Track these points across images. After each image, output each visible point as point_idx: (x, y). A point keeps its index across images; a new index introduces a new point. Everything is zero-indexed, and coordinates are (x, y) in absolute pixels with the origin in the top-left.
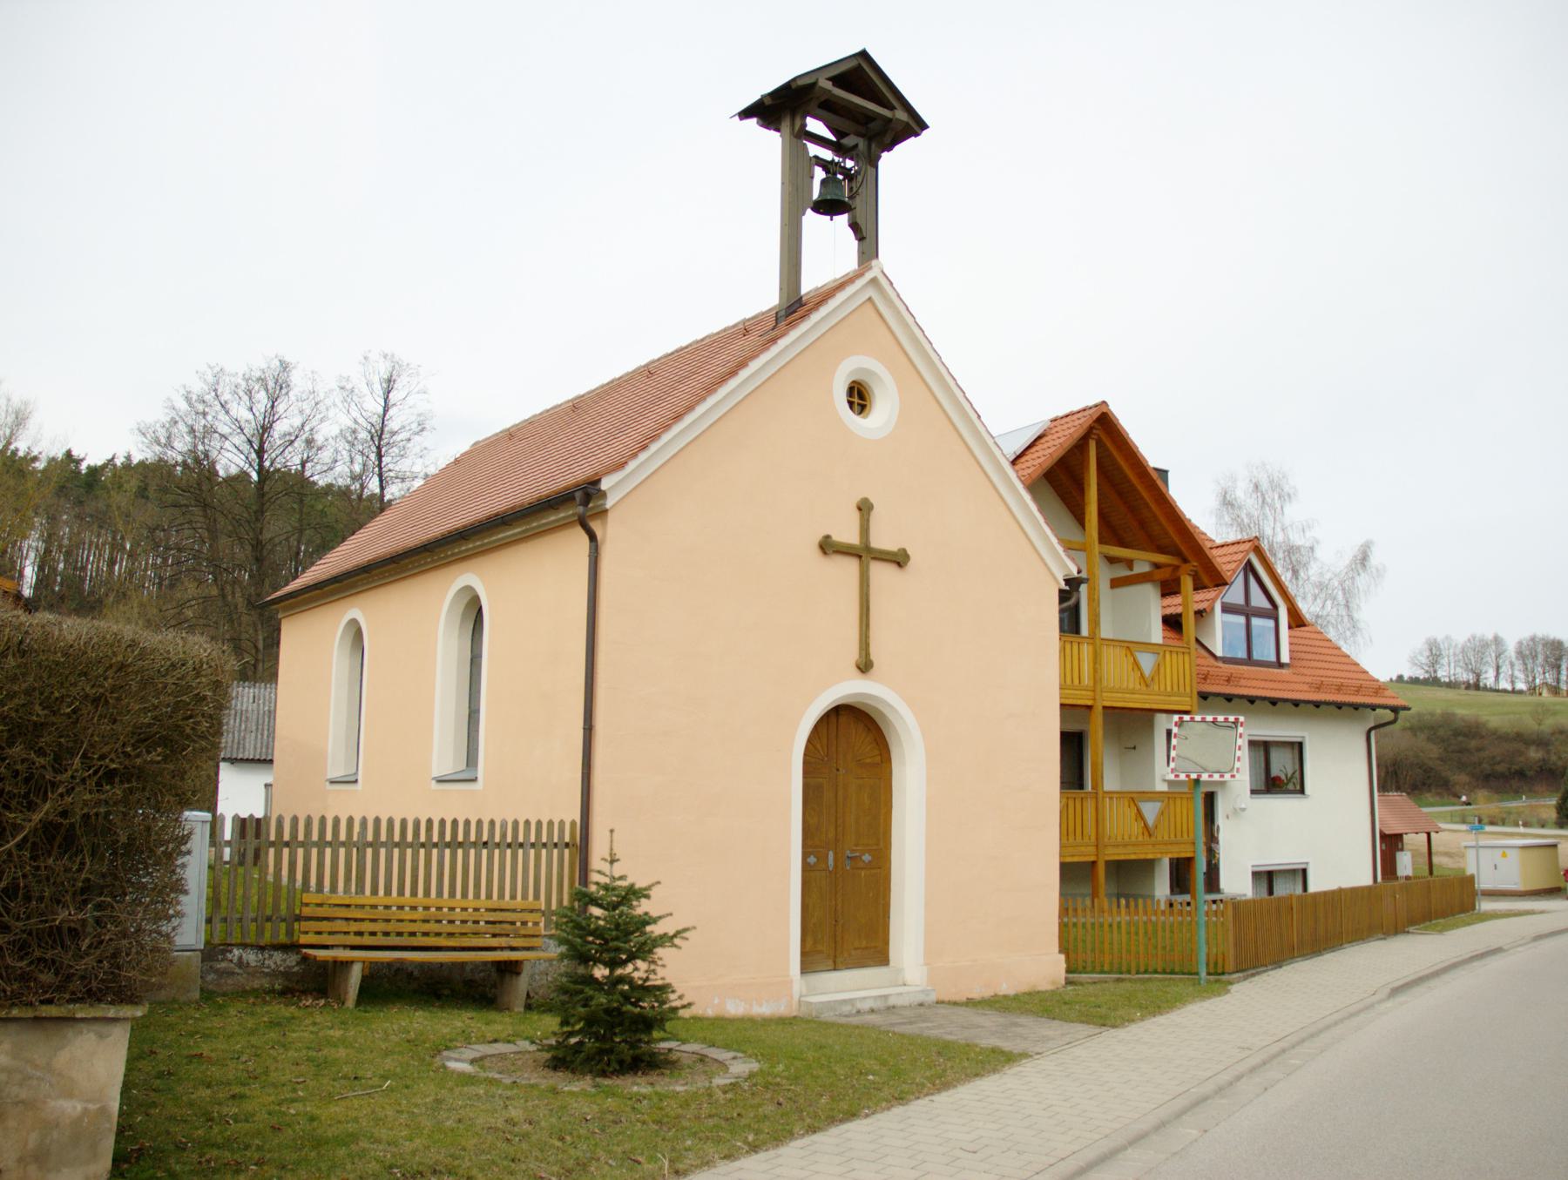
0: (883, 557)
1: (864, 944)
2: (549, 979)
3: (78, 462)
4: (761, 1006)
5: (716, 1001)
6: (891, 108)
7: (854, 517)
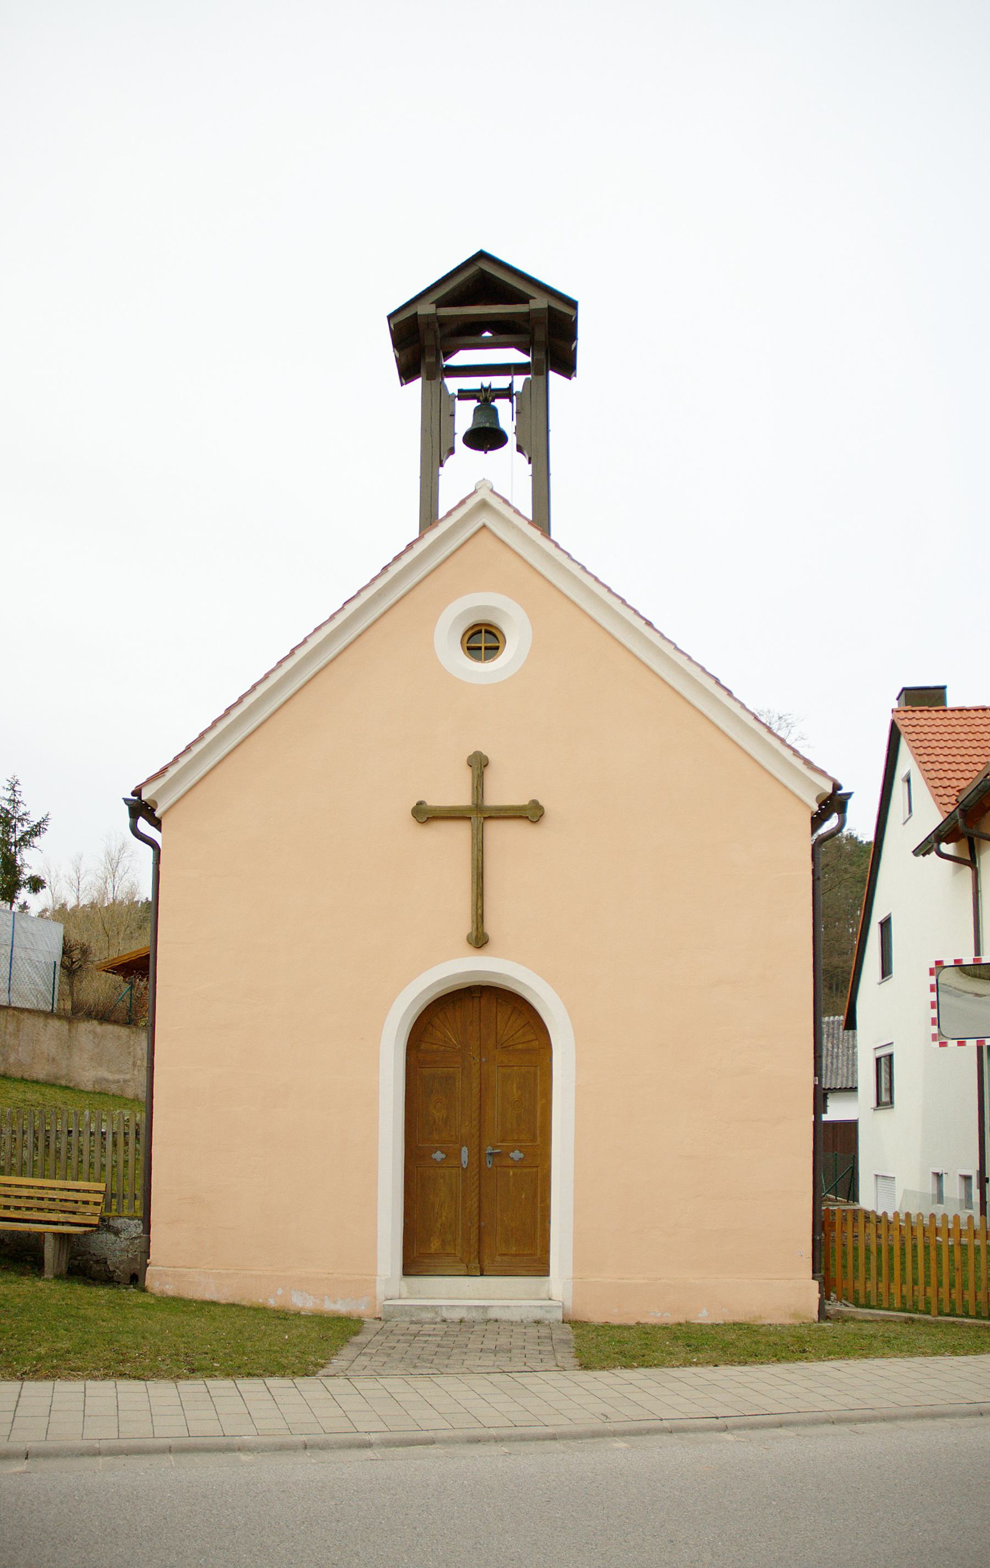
0: (875, 862)
1: (513, 1250)
2: (130, 1256)
3: (42, 889)
4: (335, 1302)
5: (280, 1292)
6: (525, 299)
7: (465, 778)
